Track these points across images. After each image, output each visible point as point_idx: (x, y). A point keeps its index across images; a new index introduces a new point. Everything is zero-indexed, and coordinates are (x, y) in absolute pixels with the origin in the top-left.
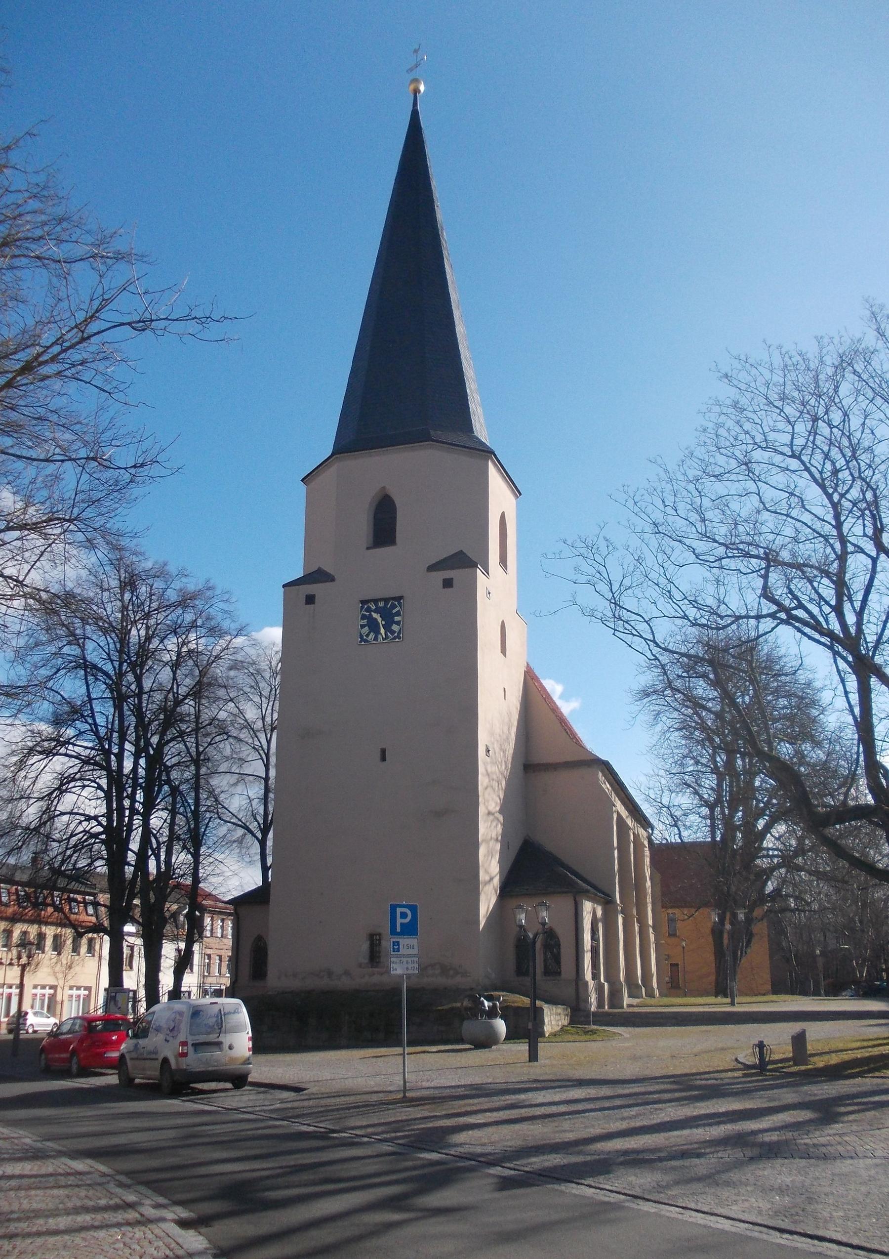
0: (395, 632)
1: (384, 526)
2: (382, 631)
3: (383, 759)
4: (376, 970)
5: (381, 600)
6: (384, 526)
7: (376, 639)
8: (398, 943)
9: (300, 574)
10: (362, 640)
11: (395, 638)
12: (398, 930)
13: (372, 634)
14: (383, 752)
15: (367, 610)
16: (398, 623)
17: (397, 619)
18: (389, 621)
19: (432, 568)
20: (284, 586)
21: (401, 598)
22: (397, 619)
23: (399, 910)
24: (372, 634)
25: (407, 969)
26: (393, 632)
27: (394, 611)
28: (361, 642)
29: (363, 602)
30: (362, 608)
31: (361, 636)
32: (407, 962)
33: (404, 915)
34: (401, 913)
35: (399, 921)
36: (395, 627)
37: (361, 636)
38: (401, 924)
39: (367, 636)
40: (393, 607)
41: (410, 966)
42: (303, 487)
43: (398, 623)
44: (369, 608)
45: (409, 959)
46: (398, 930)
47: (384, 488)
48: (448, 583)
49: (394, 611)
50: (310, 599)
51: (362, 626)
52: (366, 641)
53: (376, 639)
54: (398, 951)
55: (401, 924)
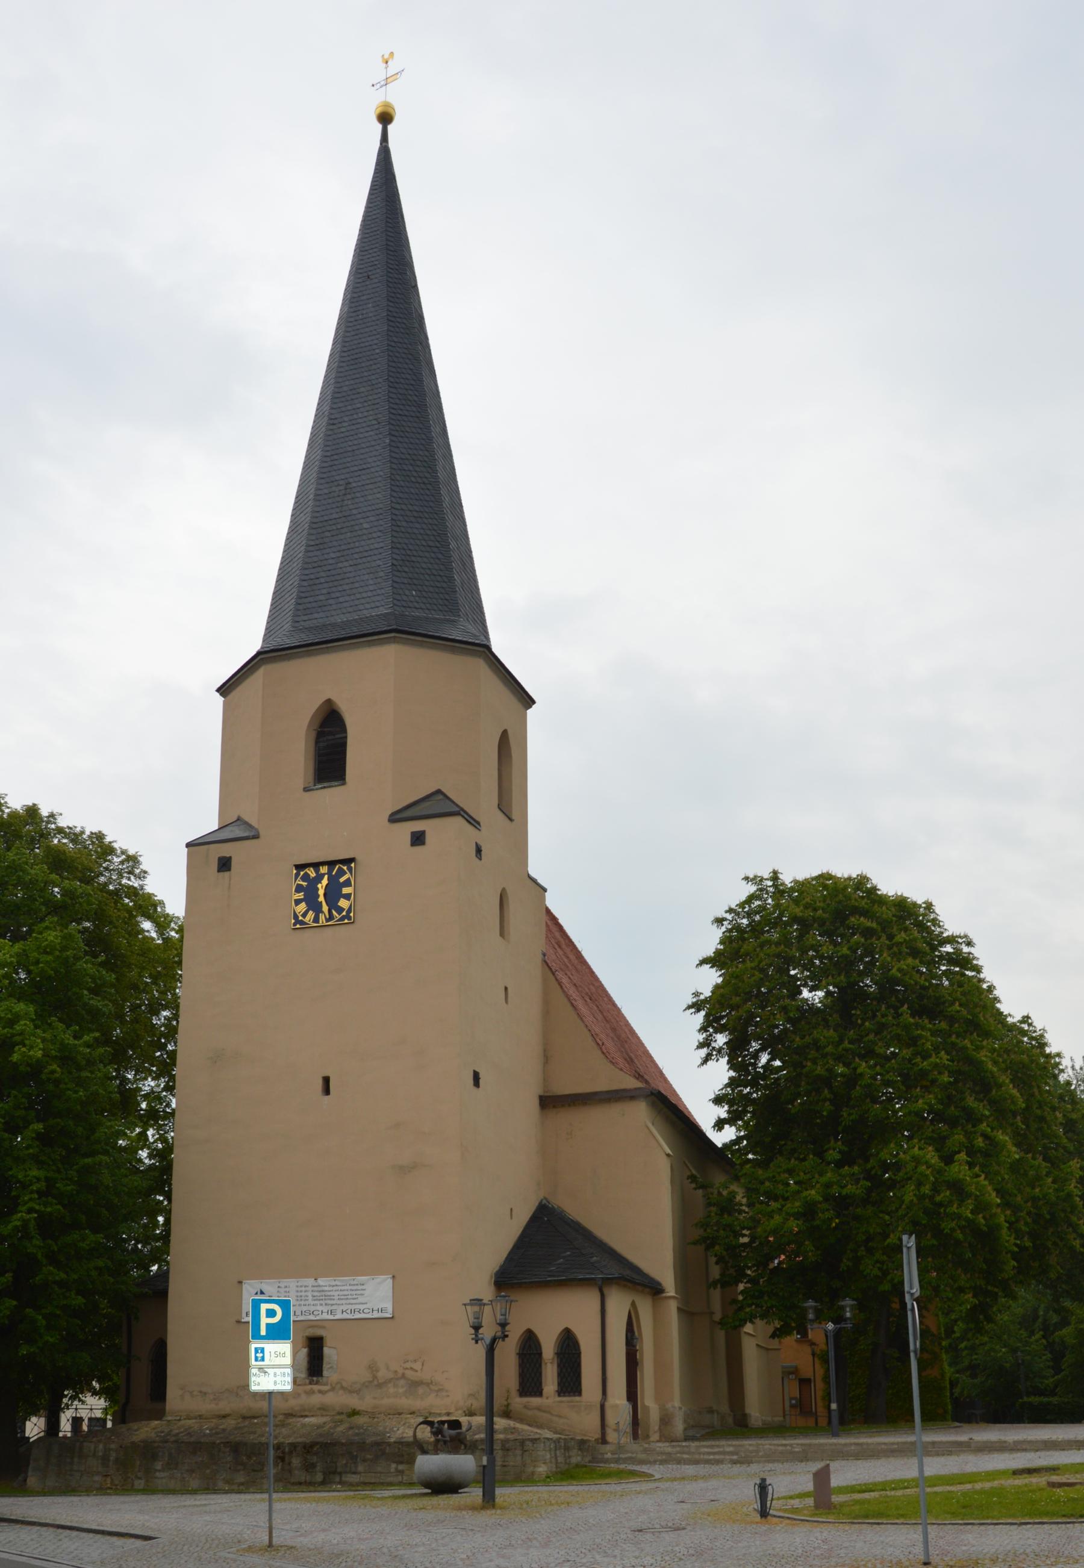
0: (343, 909)
1: (329, 759)
2: (325, 908)
3: (327, 1091)
4: (316, 1387)
5: (323, 864)
6: (329, 759)
7: (316, 920)
8: (263, 1350)
9: (216, 828)
10: (297, 921)
11: (343, 918)
12: (263, 1332)
13: (311, 912)
14: (326, 1081)
15: (303, 879)
16: (347, 897)
17: (346, 890)
18: (333, 894)
19: (396, 818)
20: (188, 845)
21: (352, 860)
22: (346, 890)
23: (264, 1307)
24: (311, 912)
25: (275, 1383)
26: (340, 910)
27: (342, 880)
28: (295, 924)
29: (299, 867)
30: (297, 875)
31: (296, 917)
32: (275, 1374)
33: (271, 1313)
34: (267, 1310)
35: (264, 1321)
36: (343, 903)
37: (296, 917)
38: (267, 1325)
39: (304, 915)
40: (341, 873)
41: (279, 1379)
42: (219, 700)
43: (347, 897)
44: (306, 876)
45: (278, 1371)
46: (263, 1332)
47: (329, 702)
48: (418, 839)
49: (342, 880)
50: (225, 864)
51: (298, 902)
52: (302, 923)
53: (316, 920)
54: (263, 1359)
55: (267, 1325)
